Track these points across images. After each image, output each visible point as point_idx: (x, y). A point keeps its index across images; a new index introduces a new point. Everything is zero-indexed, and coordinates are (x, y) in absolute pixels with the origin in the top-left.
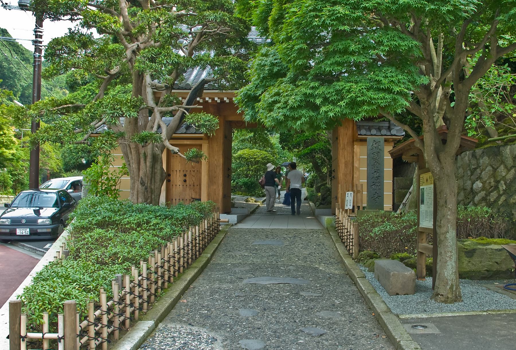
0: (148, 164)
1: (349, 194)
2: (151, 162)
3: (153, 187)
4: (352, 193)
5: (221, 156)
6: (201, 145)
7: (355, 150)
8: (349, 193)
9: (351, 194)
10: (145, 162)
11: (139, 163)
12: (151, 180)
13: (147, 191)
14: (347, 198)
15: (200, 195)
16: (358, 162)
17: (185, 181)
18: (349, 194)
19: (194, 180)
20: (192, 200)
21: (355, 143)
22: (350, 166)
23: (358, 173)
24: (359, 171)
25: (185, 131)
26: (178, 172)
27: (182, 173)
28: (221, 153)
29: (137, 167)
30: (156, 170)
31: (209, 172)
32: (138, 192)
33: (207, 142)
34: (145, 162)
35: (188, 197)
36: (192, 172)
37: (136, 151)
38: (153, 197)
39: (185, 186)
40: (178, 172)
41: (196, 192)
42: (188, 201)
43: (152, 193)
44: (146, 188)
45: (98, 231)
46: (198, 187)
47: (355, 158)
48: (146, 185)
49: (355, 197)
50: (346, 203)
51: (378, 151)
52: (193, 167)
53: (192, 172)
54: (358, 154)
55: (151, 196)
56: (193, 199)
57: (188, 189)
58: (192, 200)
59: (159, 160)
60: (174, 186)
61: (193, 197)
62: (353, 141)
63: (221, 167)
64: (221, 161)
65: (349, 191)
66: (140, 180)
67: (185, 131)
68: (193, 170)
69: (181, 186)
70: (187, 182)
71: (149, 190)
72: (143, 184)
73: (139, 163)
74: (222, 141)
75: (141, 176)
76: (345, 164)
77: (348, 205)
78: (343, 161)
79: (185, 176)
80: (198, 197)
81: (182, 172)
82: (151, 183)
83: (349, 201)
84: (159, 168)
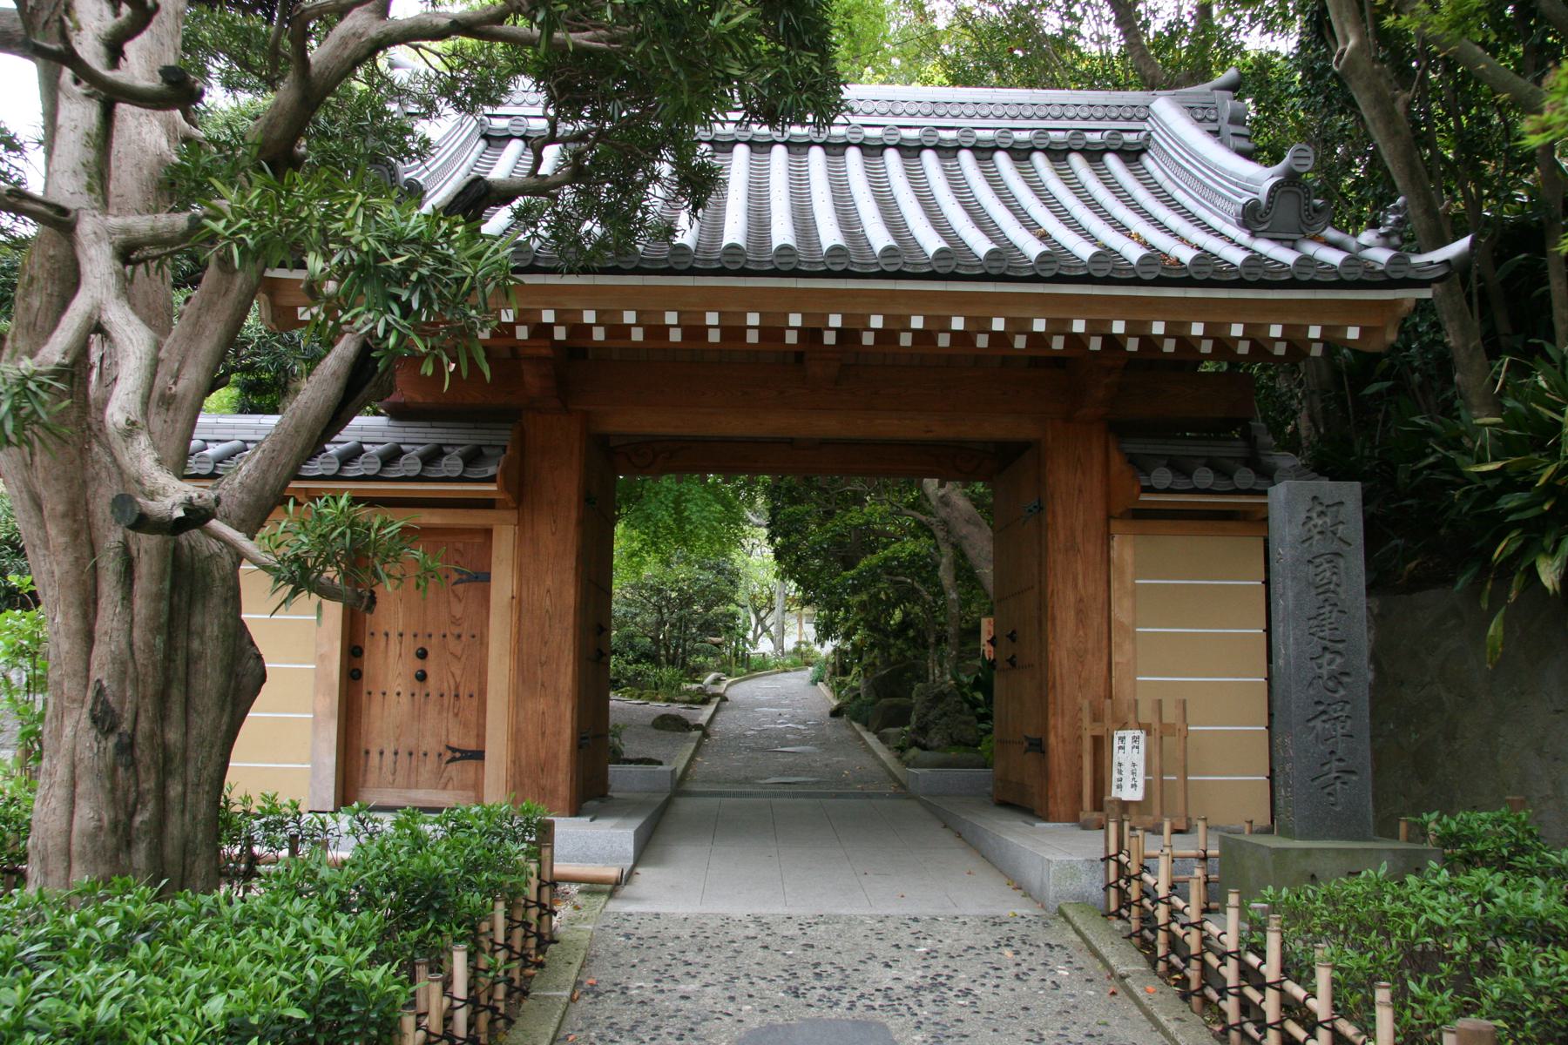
0: (141, 606)
1: (1129, 741)
2: (158, 597)
3: (173, 736)
4: (1142, 735)
5: (570, 577)
6: (488, 532)
7: (1114, 554)
8: (1129, 734)
9: (1135, 739)
10: (128, 598)
11: (88, 605)
12: (163, 697)
13: (132, 764)
14: (1118, 756)
15: (481, 737)
16: (1127, 603)
17: (422, 677)
18: (1129, 741)
19: (458, 673)
20: (449, 755)
21: (1116, 525)
22: (1096, 620)
23: (1127, 646)
24: (1134, 637)
25: (416, 468)
26: (394, 637)
27: (411, 646)
28: (570, 562)
29: (75, 624)
30: (196, 645)
31: (519, 641)
32: (73, 767)
33: (512, 516)
34: (128, 598)
35: (431, 744)
36: (451, 640)
37: (76, 535)
38: (175, 790)
39: (419, 697)
40: (394, 637)
41: (465, 725)
42: (433, 758)
43: (164, 770)
44: (126, 748)
45: (188, 816)
46: (475, 702)
47: (1115, 585)
48: (126, 726)
49: (1156, 750)
50: (1115, 775)
51: (1335, 546)
52: (455, 622)
53: (451, 640)
54: (1129, 570)
55: (162, 789)
56: (454, 750)
57: (432, 710)
58: (449, 755)
59: (218, 589)
60: (377, 697)
61: (454, 742)
62: (1109, 517)
63: (570, 619)
64: (570, 596)
65: (1124, 726)
66: (90, 694)
67: (416, 468)
68: (457, 631)
69: (405, 699)
70: (431, 679)
71: (143, 753)
72: (104, 720)
73: (88, 605)
74: (574, 514)
75: (96, 674)
76: (1079, 612)
77: (1127, 783)
78: (1071, 597)
79: (422, 654)
80: (471, 744)
81: (408, 639)
82: (162, 716)
83: (1127, 768)
84: (213, 629)
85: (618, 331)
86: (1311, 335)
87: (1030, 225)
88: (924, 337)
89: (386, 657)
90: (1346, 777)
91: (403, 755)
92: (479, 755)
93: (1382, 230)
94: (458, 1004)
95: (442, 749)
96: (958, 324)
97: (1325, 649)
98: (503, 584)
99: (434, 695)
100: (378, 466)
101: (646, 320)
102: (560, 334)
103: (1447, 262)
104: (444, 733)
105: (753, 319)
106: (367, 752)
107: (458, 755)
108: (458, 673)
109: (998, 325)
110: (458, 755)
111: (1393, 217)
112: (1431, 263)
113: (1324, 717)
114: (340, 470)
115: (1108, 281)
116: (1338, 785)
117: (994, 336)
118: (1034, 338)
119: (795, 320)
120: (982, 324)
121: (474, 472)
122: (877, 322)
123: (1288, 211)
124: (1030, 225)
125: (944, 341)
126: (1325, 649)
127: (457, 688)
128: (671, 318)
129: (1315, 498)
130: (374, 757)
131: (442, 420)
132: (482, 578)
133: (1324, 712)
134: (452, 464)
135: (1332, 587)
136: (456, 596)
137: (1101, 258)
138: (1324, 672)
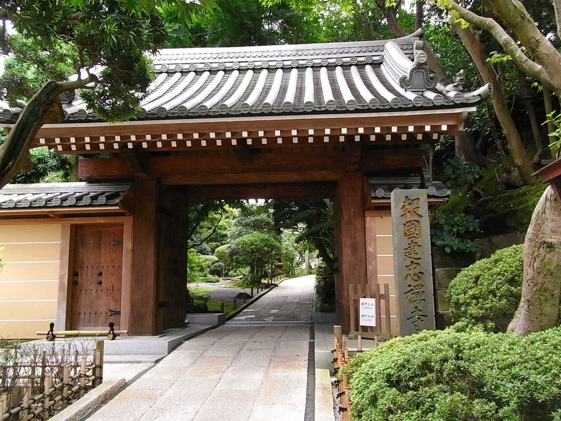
17: (100, 283)
19: (113, 281)
20: (110, 313)
26: (90, 267)
42: (104, 314)
58: (110, 313)
60: (84, 292)
61: (112, 308)
70: (103, 284)
79: (100, 274)
85: (272, 140)
86: (276, 135)
87: (369, 86)
88: (349, 138)
89: (87, 275)
90: (422, 318)
91: (93, 313)
92: (119, 313)
93: (455, 84)
94: (45, 396)
95: (107, 311)
96: (378, 130)
97: (412, 262)
98: (128, 244)
99: (104, 290)
100: (90, 201)
101: (269, 135)
102: (249, 142)
103: (479, 95)
104: (108, 304)
105: (311, 132)
106: (80, 313)
107: (113, 313)
108: (113, 281)
109: (394, 129)
110: (113, 313)
111: (458, 78)
112: (474, 96)
113: (413, 292)
114: (61, 203)
115: (400, 109)
116: (419, 321)
117: (393, 135)
118: (410, 135)
119: (328, 131)
120: (188, 136)
121: (111, 202)
122: (344, 131)
123: (419, 79)
124: (369, 86)
125: (373, 138)
126: (412, 262)
127: (113, 286)
128: (278, 133)
129: (406, 197)
130: (82, 315)
131: (105, 182)
132: (121, 243)
133: (412, 290)
134: (102, 200)
135: (415, 235)
136: (113, 251)
137: (417, 99)
138: (411, 272)
